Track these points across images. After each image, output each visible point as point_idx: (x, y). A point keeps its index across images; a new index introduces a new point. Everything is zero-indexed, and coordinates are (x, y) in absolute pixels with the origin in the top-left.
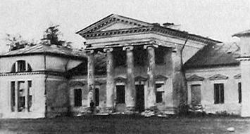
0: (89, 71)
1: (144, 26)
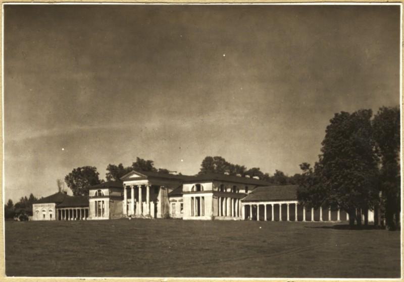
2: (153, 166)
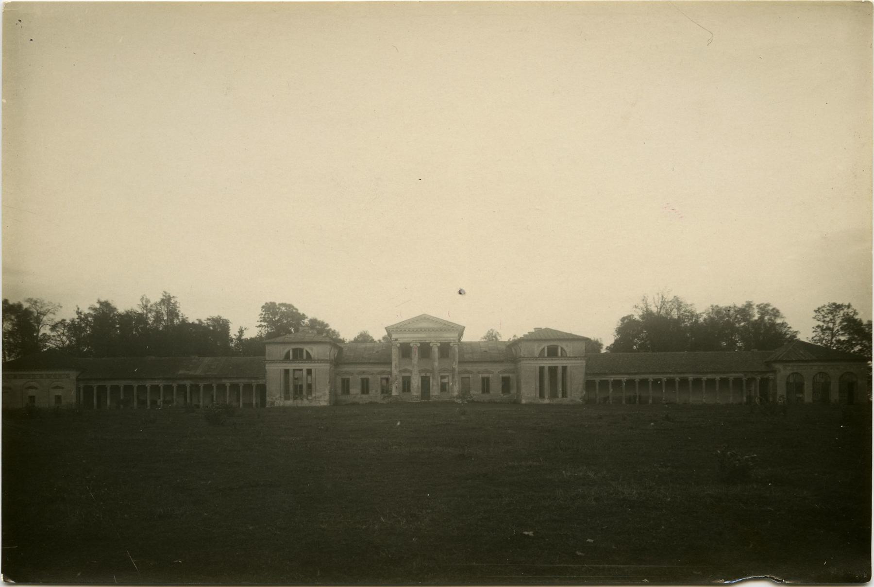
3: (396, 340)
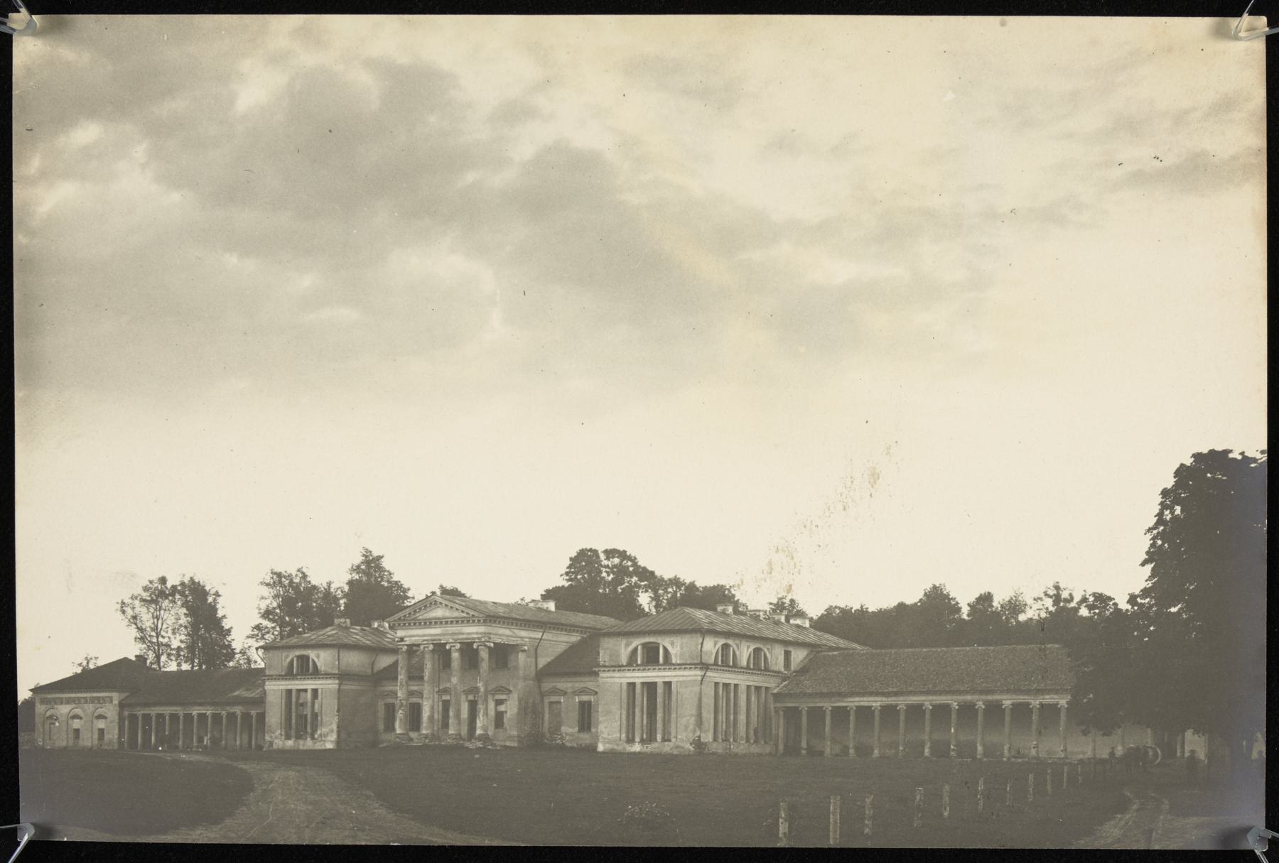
0: (400, 677)
1: (473, 616)
2: (870, 610)
3: (402, 639)
